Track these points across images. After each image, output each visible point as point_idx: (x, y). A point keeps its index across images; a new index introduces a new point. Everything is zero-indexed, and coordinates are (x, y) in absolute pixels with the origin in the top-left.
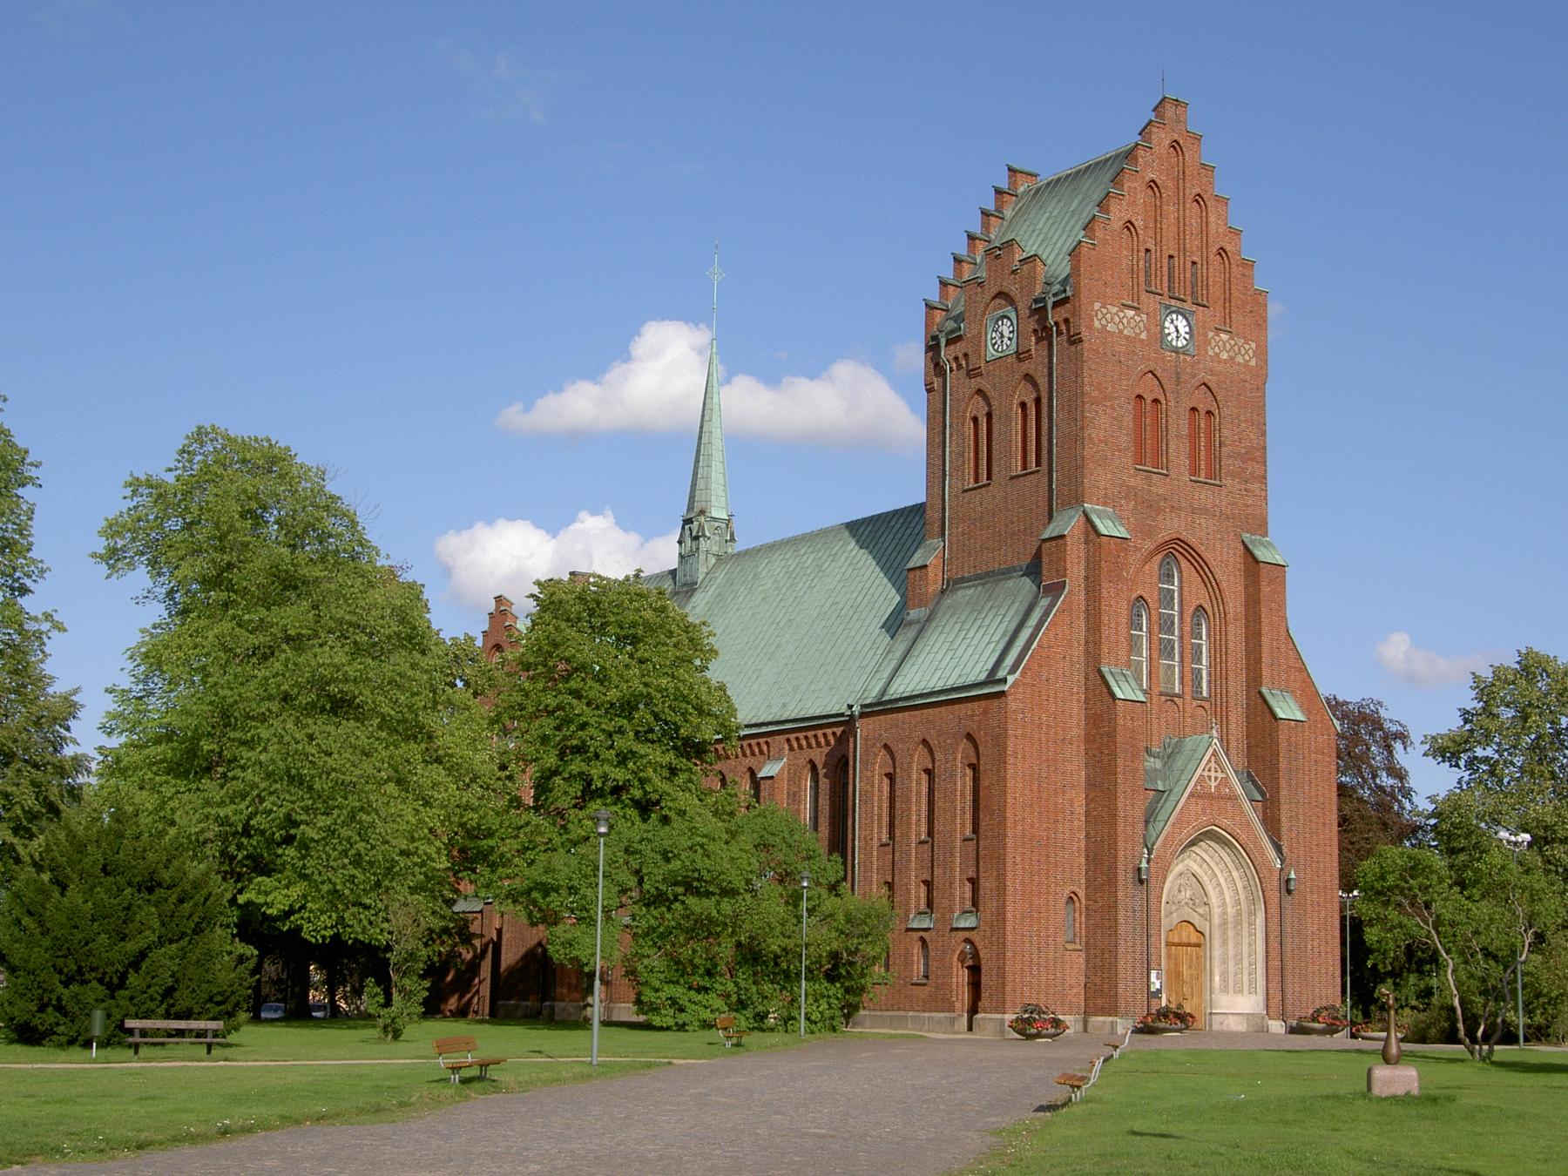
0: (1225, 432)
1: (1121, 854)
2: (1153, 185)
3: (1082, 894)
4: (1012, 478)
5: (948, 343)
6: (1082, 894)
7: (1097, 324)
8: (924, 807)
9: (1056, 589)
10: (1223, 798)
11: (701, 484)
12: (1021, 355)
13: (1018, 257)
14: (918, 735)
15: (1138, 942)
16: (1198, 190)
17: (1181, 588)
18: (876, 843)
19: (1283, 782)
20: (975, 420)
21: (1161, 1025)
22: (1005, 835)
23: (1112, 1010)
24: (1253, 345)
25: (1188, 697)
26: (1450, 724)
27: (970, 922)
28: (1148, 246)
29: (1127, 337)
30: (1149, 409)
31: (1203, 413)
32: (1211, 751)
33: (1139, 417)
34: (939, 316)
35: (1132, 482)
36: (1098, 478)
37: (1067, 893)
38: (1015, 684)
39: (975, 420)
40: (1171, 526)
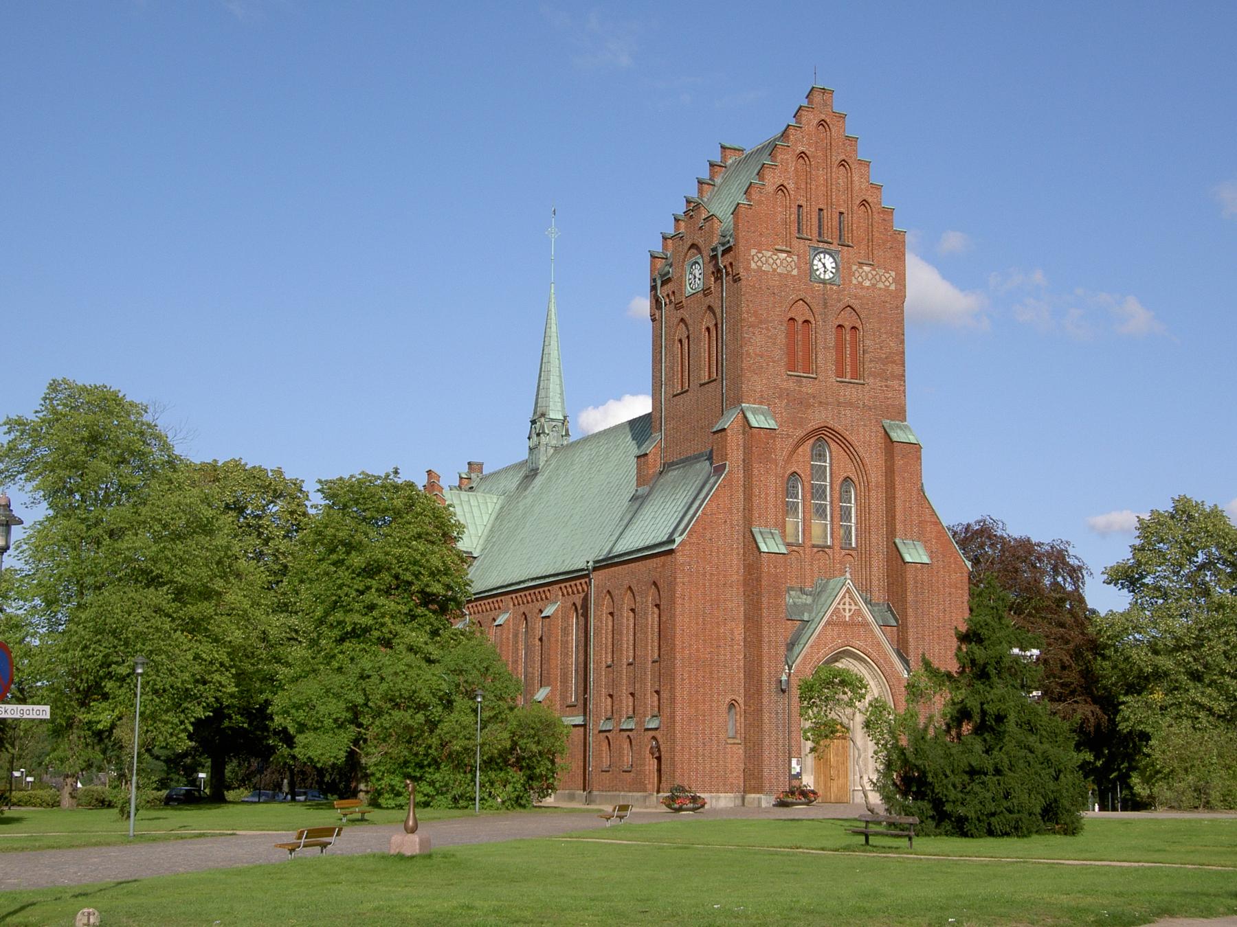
0: (868, 342)
1: (766, 670)
2: (802, 155)
3: (741, 701)
4: (701, 385)
5: (663, 283)
6: (741, 701)
7: (753, 265)
8: (631, 638)
9: (719, 470)
10: (857, 624)
11: (542, 393)
12: (706, 292)
13: (704, 216)
14: (626, 583)
15: (781, 736)
16: (843, 157)
17: (831, 465)
18: (604, 666)
19: (910, 611)
20: (680, 341)
21: (790, 800)
22: (675, 658)
23: (759, 789)
24: (893, 274)
25: (837, 548)
26: (1122, 554)
27: (631, 725)
28: (800, 203)
29: (780, 274)
30: (799, 331)
31: (848, 329)
32: (844, 589)
33: (791, 335)
34: (659, 264)
35: (785, 385)
36: (755, 383)
37: (728, 700)
38: (682, 543)
39: (680, 341)
40: (818, 417)
